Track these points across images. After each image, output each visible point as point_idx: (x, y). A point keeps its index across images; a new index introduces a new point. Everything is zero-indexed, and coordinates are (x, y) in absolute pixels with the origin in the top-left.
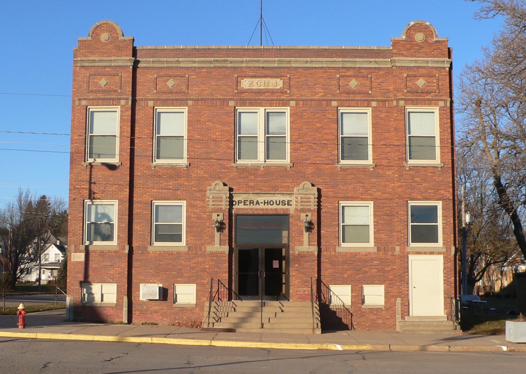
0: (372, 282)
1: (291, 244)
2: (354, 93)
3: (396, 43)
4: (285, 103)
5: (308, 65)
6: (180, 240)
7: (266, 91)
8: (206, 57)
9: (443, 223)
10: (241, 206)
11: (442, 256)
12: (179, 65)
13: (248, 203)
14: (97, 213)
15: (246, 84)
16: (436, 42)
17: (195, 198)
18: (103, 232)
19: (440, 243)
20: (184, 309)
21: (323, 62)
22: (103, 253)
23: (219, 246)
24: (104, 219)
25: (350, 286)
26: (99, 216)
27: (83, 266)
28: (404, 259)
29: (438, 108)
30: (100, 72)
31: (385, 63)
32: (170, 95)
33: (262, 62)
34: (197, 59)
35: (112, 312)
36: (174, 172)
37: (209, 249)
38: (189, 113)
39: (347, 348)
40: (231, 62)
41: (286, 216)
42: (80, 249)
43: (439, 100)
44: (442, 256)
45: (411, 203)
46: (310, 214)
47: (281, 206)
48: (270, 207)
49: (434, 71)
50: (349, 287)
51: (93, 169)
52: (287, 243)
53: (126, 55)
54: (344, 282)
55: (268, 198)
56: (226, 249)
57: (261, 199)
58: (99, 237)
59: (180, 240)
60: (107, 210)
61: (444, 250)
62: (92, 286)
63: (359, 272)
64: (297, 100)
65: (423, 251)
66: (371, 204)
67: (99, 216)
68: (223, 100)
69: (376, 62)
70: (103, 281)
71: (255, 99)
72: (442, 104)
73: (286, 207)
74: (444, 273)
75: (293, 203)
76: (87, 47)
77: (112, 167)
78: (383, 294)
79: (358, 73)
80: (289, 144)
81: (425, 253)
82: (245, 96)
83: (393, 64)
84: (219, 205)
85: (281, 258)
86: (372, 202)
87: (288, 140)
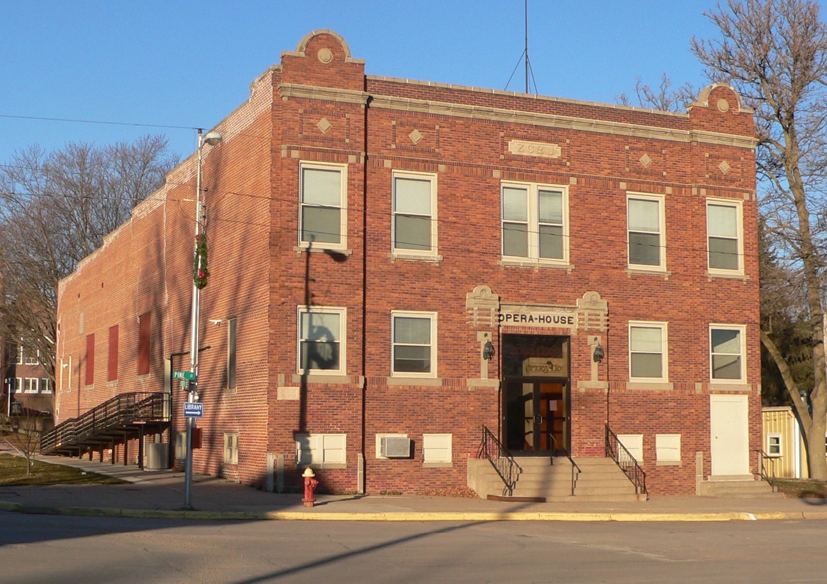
0: (667, 431)
1: (572, 377)
2: (646, 173)
3: (695, 111)
4: (565, 181)
5: (592, 129)
6: (427, 369)
7: (541, 160)
8: (461, 102)
9: (748, 354)
10: (511, 322)
11: (746, 398)
12: (426, 110)
13: (519, 318)
14: (311, 327)
15: (515, 147)
16: (741, 113)
17: (452, 309)
18: (322, 355)
19: (744, 380)
20: (436, 471)
21: (610, 127)
22: (328, 389)
23: (486, 380)
24: (322, 336)
25: (642, 436)
26: (315, 330)
27: (297, 408)
28: (705, 399)
29: (741, 202)
30: (317, 109)
31: (682, 136)
32: (414, 153)
33: (538, 118)
34: (452, 105)
35: (341, 477)
36: (422, 269)
37: (472, 383)
38: (439, 182)
39: (760, 517)
40: (497, 114)
41: (566, 338)
42: (294, 381)
43: (743, 191)
44: (747, 396)
45: (713, 326)
46: (599, 337)
47: (559, 325)
48: (546, 325)
49: (739, 153)
50: (678, 437)
51: (311, 259)
52: (566, 375)
53: (355, 87)
54: (636, 431)
55: (544, 313)
56: (495, 383)
57: (536, 314)
58: (314, 364)
59: (427, 369)
60: (328, 322)
61: (750, 389)
62: (309, 439)
63: (651, 416)
64: (578, 177)
65: (726, 389)
66: (664, 325)
67: (315, 330)
68: (487, 167)
69: (672, 133)
70: (326, 430)
71: (528, 169)
72: (352, 159)
73: (567, 325)
74: (749, 419)
75: (576, 320)
76: (290, 68)
77: (338, 257)
78: (679, 447)
79: (651, 146)
80: (568, 238)
81: (729, 393)
82: (514, 165)
83: (694, 139)
84: (486, 320)
85: (558, 396)
86: (666, 323)
87: (566, 231)
